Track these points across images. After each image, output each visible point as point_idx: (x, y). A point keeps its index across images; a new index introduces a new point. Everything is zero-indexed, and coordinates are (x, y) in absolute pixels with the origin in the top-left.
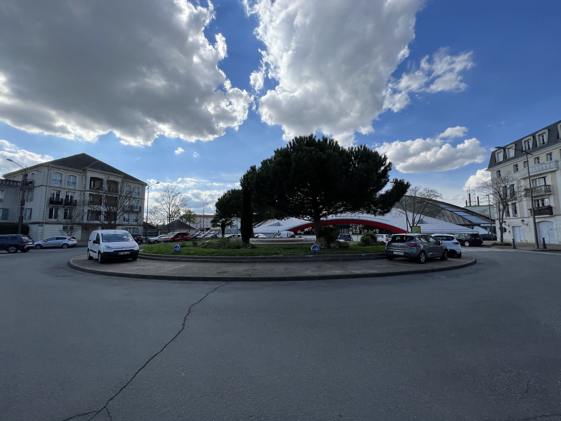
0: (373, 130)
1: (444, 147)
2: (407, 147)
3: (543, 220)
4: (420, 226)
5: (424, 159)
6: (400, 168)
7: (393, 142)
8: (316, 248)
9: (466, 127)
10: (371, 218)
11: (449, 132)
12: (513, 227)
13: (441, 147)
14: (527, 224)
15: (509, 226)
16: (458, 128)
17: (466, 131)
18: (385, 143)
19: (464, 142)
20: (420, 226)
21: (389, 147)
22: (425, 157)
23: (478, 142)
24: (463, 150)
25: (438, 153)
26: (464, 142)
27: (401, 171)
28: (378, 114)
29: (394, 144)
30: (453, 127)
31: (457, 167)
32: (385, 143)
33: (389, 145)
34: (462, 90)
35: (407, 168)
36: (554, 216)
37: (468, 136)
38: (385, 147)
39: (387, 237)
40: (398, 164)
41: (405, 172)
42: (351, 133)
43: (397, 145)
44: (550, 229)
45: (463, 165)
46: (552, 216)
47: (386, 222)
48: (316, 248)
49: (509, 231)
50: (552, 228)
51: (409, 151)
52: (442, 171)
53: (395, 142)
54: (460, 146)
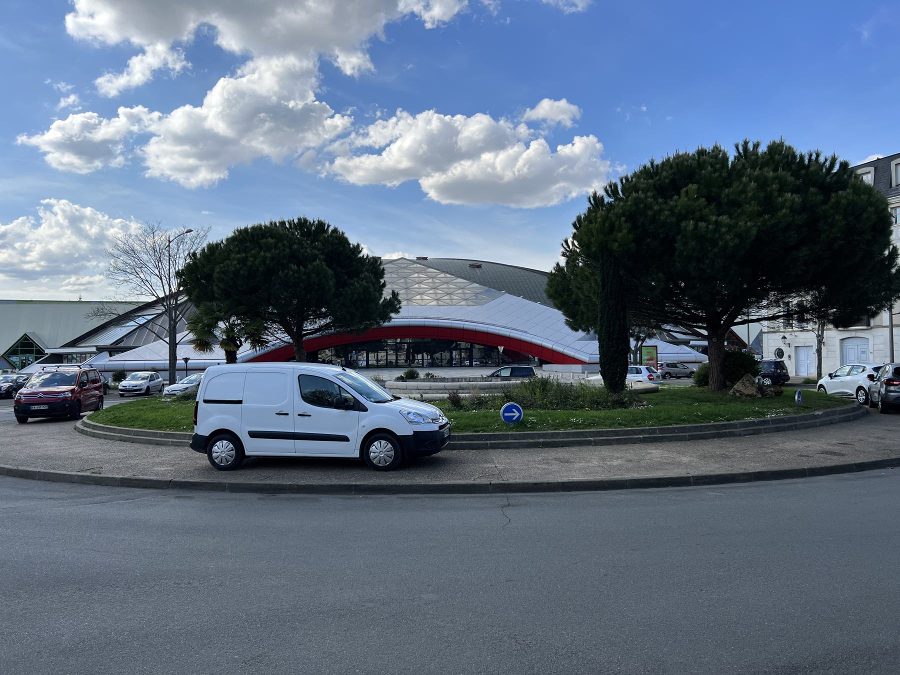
0: (370, 66)
1: (534, 145)
2: (452, 132)
3: (853, 334)
4: (656, 346)
5: (489, 170)
6: (431, 187)
7: (420, 111)
8: (514, 412)
9: (580, 107)
10: (472, 324)
11: (546, 108)
12: (796, 347)
13: (527, 146)
14: (789, 344)
15: (789, 346)
16: (563, 103)
17: (400, 109)
18: (401, 112)
19: (573, 142)
20: (656, 346)
21: (410, 125)
22: (493, 166)
23: (599, 146)
24: (571, 161)
25: (520, 163)
26: (573, 142)
27: (433, 194)
28: (384, 22)
29: (422, 117)
30: (555, 100)
31: (555, 202)
32: (401, 112)
33: (410, 120)
34: (580, 9)
35: (447, 189)
36: (871, 328)
37: (582, 128)
38: (401, 123)
39: (650, 372)
40: (428, 175)
41: (445, 202)
42: (308, 64)
43: (429, 122)
44: (862, 352)
45: (566, 197)
46: (869, 327)
47: (499, 330)
48: (514, 412)
49: (789, 357)
50: (864, 350)
51: (456, 143)
52: (526, 206)
53: (426, 112)
54: (564, 150)
